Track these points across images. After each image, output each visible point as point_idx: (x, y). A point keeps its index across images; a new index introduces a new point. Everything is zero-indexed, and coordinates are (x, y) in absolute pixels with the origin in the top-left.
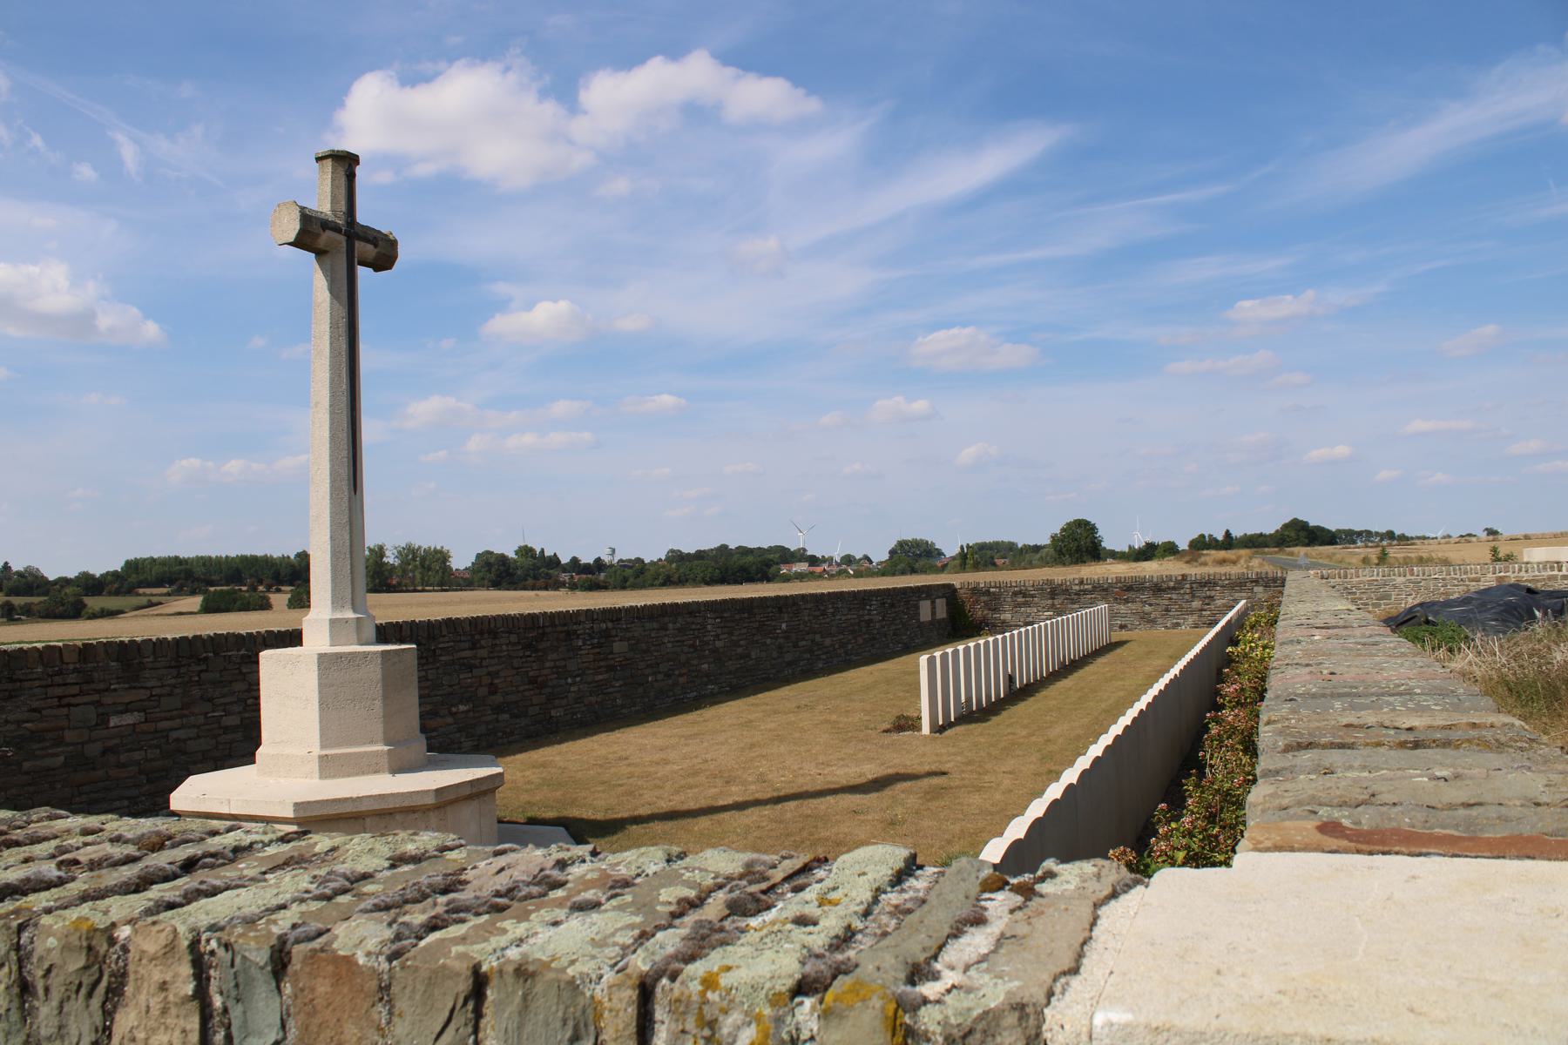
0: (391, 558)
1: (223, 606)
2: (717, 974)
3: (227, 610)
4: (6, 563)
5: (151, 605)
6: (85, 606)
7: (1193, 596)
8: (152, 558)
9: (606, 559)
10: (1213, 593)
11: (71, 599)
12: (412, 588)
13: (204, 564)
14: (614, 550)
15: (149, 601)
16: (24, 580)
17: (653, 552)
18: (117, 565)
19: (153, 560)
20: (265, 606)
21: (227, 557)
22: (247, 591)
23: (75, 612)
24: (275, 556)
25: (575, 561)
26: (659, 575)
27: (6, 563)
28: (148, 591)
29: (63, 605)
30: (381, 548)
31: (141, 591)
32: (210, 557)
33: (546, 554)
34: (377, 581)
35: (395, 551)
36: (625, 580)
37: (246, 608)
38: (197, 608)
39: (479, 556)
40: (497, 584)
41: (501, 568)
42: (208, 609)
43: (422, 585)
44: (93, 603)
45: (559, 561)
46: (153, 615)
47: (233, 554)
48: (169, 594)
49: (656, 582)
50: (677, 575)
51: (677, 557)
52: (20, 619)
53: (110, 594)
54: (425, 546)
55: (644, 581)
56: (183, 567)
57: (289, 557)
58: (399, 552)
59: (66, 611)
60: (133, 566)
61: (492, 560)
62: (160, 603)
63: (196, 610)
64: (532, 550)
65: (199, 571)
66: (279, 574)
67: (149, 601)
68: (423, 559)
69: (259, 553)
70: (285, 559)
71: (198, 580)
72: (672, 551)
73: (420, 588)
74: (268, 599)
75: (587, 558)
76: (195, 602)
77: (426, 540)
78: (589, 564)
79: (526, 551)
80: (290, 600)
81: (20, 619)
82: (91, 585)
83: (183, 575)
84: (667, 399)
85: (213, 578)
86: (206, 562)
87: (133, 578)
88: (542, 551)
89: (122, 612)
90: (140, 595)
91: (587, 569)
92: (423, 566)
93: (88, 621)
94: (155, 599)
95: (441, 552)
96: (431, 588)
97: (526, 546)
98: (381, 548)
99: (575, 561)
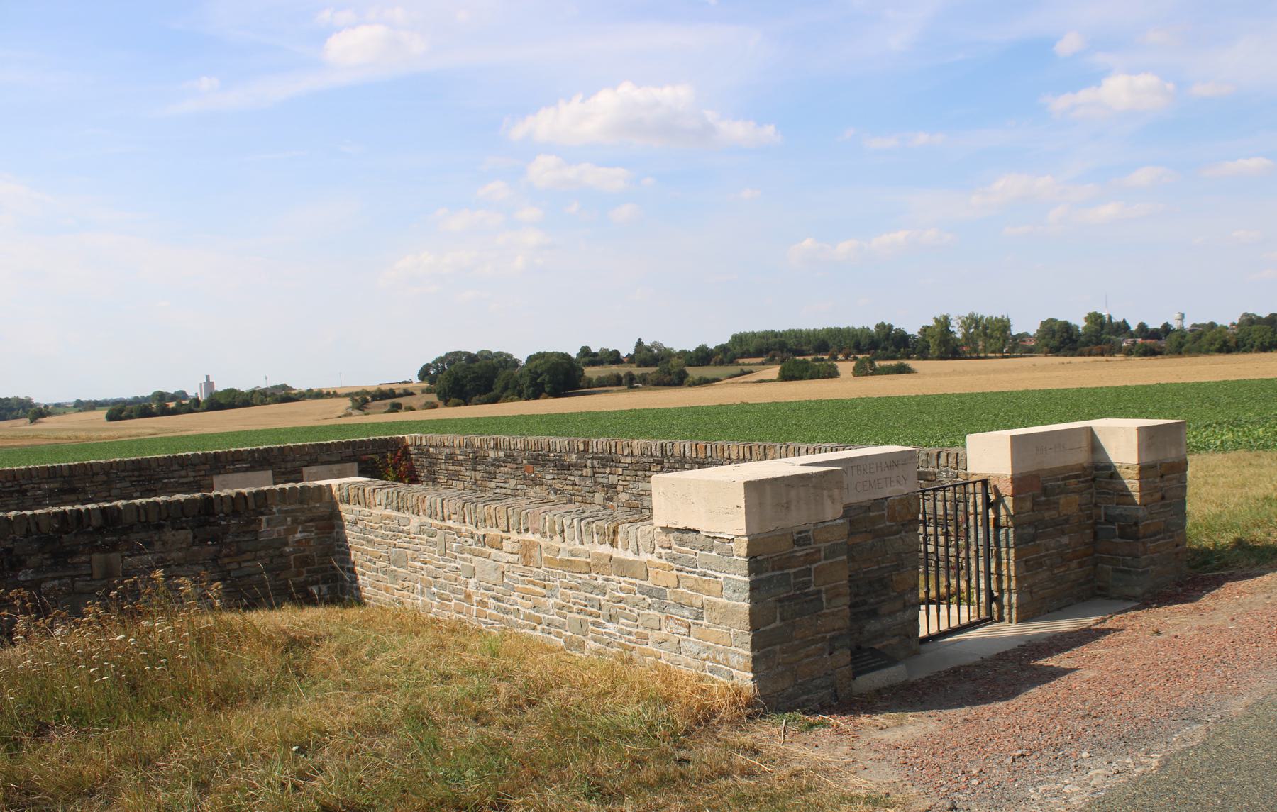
0: (957, 331)
1: (797, 374)
2: (286, 538)
3: (800, 378)
4: (640, 340)
5: (744, 373)
6: (687, 375)
7: (595, 483)
8: (753, 333)
9: (1175, 325)
10: (614, 479)
11: (676, 370)
12: (975, 355)
13: (796, 337)
14: (1183, 316)
15: (742, 370)
16: (650, 353)
17: (1227, 317)
18: (725, 339)
19: (754, 334)
20: (833, 374)
21: (815, 330)
22: (829, 360)
23: (679, 380)
24: (857, 328)
25: (1142, 327)
26: (1215, 340)
27: (640, 340)
28: (746, 361)
29: (670, 375)
30: (946, 318)
31: (740, 361)
32: (801, 331)
33: (1114, 321)
34: (943, 349)
35: (959, 321)
36: (1181, 345)
37: (815, 376)
38: (775, 376)
39: (1043, 324)
40: (1056, 351)
41: (1065, 335)
42: (785, 377)
43: (985, 352)
44: (694, 372)
45: (1128, 327)
46: (743, 383)
47: (820, 327)
48: (763, 364)
49: (1213, 348)
50: (1234, 340)
51: (1250, 321)
52: (637, 387)
53: (716, 364)
54: (987, 315)
55: (1201, 347)
56: (777, 340)
57: (868, 329)
58: (963, 322)
59: (672, 380)
60: (738, 339)
61: (1056, 328)
62: (752, 372)
63: (775, 378)
64: (1101, 316)
65: (791, 343)
66: (860, 344)
67: (742, 370)
68: (986, 328)
69: (843, 326)
70: (865, 331)
71: (790, 350)
72: (1246, 315)
73: (982, 355)
74: (835, 368)
75: (1154, 324)
76: (773, 372)
77: (989, 310)
78: (1157, 329)
79: (1095, 319)
80: (854, 369)
81: (637, 387)
82: (703, 357)
83: (777, 346)
84: (1254, 163)
85: (804, 348)
86: (797, 335)
87: (738, 350)
88: (1110, 317)
89: (718, 380)
90: (740, 365)
91: (1155, 334)
92: (985, 334)
93: (690, 389)
94: (746, 369)
95: (1002, 320)
96: (993, 355)
97: (1096, 313)
98: (946, 318)
99: (1142, 327)
